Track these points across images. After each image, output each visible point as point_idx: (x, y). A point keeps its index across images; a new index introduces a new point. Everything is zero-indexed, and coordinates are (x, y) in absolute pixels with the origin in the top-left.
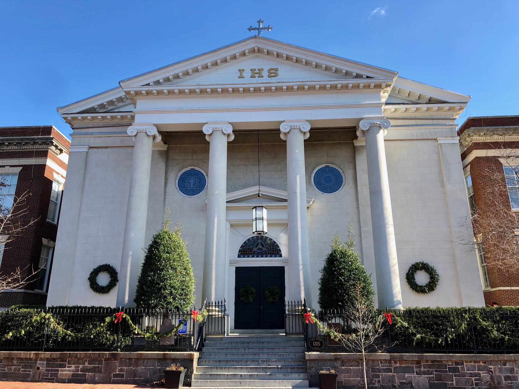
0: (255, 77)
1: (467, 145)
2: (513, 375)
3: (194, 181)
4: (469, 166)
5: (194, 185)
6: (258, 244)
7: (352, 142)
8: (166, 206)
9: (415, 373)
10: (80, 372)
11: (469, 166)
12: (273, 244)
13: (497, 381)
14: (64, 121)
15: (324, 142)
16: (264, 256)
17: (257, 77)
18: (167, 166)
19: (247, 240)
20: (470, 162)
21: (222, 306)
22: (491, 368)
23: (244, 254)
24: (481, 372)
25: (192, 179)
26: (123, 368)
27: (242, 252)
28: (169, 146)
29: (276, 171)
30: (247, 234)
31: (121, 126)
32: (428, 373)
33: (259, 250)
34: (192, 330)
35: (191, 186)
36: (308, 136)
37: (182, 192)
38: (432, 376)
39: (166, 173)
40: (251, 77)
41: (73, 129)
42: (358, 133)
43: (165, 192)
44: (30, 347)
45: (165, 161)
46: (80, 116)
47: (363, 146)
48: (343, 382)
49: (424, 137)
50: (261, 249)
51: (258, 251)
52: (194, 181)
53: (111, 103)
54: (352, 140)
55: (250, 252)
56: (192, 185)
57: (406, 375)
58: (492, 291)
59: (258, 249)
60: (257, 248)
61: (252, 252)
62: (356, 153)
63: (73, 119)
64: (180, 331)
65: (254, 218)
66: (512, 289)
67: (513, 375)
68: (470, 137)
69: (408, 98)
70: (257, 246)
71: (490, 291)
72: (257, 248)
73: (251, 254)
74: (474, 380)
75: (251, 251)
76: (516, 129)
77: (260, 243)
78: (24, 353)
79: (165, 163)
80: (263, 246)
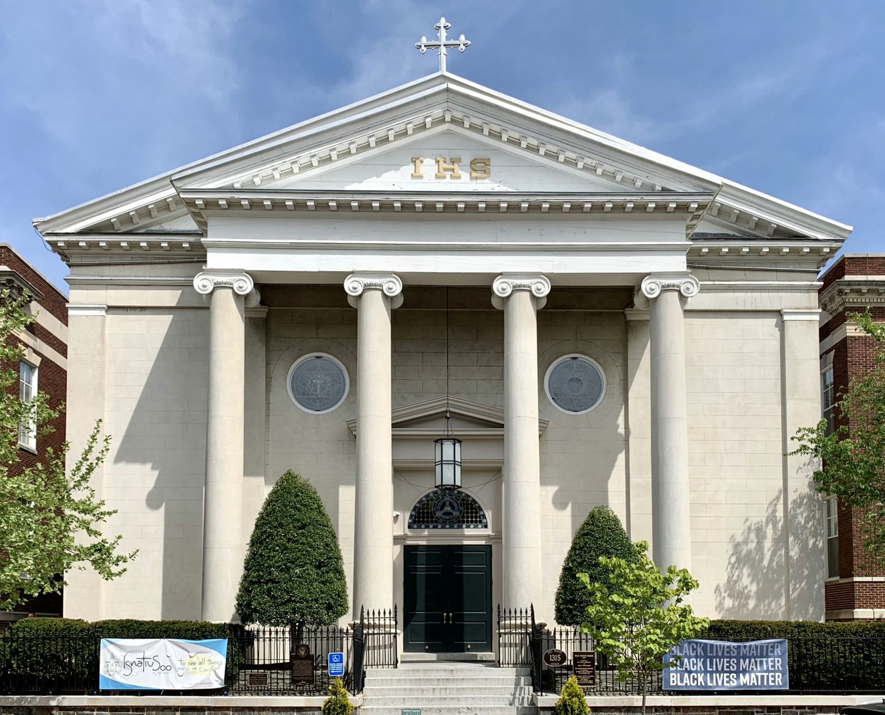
0: (444, 177)
1: (834, 311)
3: (322, 382)
4: (833, 352)
5: (322, 389)
6: (444, 505)
7: (624, 312)
8: (270, 430)
11: (833, 352)
12: (471, 504)
14: (50, 248)
15: (570, 310)
16: (456, 526)
17: (448, 177)
18: (267, 350)
19: (425, 497)
20: (837, 344)
23: (419, 522)
25: (319, 377)
27: (415, 518)
28: (269, 310)
29: (479, 365)
30: (424, 488)
31: (169, 263)
33: (446, 515)
35: (316, 392)
36: (544, 303)
37: (299, 403)
39: (268, 364)
40: (437, 177)
41: (70, 266)
42: (637, 301)
43: (268, 403)
45: (264, 340)
46: (83, 241)
47: (645, 320)
48: (426, 554)
49: (756, 307)
50: (450, 514)
51: (444, 517)
52: (322, 382)
53: (146, 212)
54: (624, 309)
55: (430, 520)
56: (318, 390)
58: (840, 584)
59: (445, 514)
60: (443, 512)
61: (434, 519)
62: (629, 335)
63: (69, 244)
64: (333, 672)
65: (438, 459)
66: (874, 580)
68: (840, 296)
69: (735, 223)
70: (442, 508)
71: (837, 583)
72: (443, 512)
73: (432, 522)
75: (432, 517)
77: (448, 503)
78: (31, 698)
79: (265, 345)
80: (453, 508)
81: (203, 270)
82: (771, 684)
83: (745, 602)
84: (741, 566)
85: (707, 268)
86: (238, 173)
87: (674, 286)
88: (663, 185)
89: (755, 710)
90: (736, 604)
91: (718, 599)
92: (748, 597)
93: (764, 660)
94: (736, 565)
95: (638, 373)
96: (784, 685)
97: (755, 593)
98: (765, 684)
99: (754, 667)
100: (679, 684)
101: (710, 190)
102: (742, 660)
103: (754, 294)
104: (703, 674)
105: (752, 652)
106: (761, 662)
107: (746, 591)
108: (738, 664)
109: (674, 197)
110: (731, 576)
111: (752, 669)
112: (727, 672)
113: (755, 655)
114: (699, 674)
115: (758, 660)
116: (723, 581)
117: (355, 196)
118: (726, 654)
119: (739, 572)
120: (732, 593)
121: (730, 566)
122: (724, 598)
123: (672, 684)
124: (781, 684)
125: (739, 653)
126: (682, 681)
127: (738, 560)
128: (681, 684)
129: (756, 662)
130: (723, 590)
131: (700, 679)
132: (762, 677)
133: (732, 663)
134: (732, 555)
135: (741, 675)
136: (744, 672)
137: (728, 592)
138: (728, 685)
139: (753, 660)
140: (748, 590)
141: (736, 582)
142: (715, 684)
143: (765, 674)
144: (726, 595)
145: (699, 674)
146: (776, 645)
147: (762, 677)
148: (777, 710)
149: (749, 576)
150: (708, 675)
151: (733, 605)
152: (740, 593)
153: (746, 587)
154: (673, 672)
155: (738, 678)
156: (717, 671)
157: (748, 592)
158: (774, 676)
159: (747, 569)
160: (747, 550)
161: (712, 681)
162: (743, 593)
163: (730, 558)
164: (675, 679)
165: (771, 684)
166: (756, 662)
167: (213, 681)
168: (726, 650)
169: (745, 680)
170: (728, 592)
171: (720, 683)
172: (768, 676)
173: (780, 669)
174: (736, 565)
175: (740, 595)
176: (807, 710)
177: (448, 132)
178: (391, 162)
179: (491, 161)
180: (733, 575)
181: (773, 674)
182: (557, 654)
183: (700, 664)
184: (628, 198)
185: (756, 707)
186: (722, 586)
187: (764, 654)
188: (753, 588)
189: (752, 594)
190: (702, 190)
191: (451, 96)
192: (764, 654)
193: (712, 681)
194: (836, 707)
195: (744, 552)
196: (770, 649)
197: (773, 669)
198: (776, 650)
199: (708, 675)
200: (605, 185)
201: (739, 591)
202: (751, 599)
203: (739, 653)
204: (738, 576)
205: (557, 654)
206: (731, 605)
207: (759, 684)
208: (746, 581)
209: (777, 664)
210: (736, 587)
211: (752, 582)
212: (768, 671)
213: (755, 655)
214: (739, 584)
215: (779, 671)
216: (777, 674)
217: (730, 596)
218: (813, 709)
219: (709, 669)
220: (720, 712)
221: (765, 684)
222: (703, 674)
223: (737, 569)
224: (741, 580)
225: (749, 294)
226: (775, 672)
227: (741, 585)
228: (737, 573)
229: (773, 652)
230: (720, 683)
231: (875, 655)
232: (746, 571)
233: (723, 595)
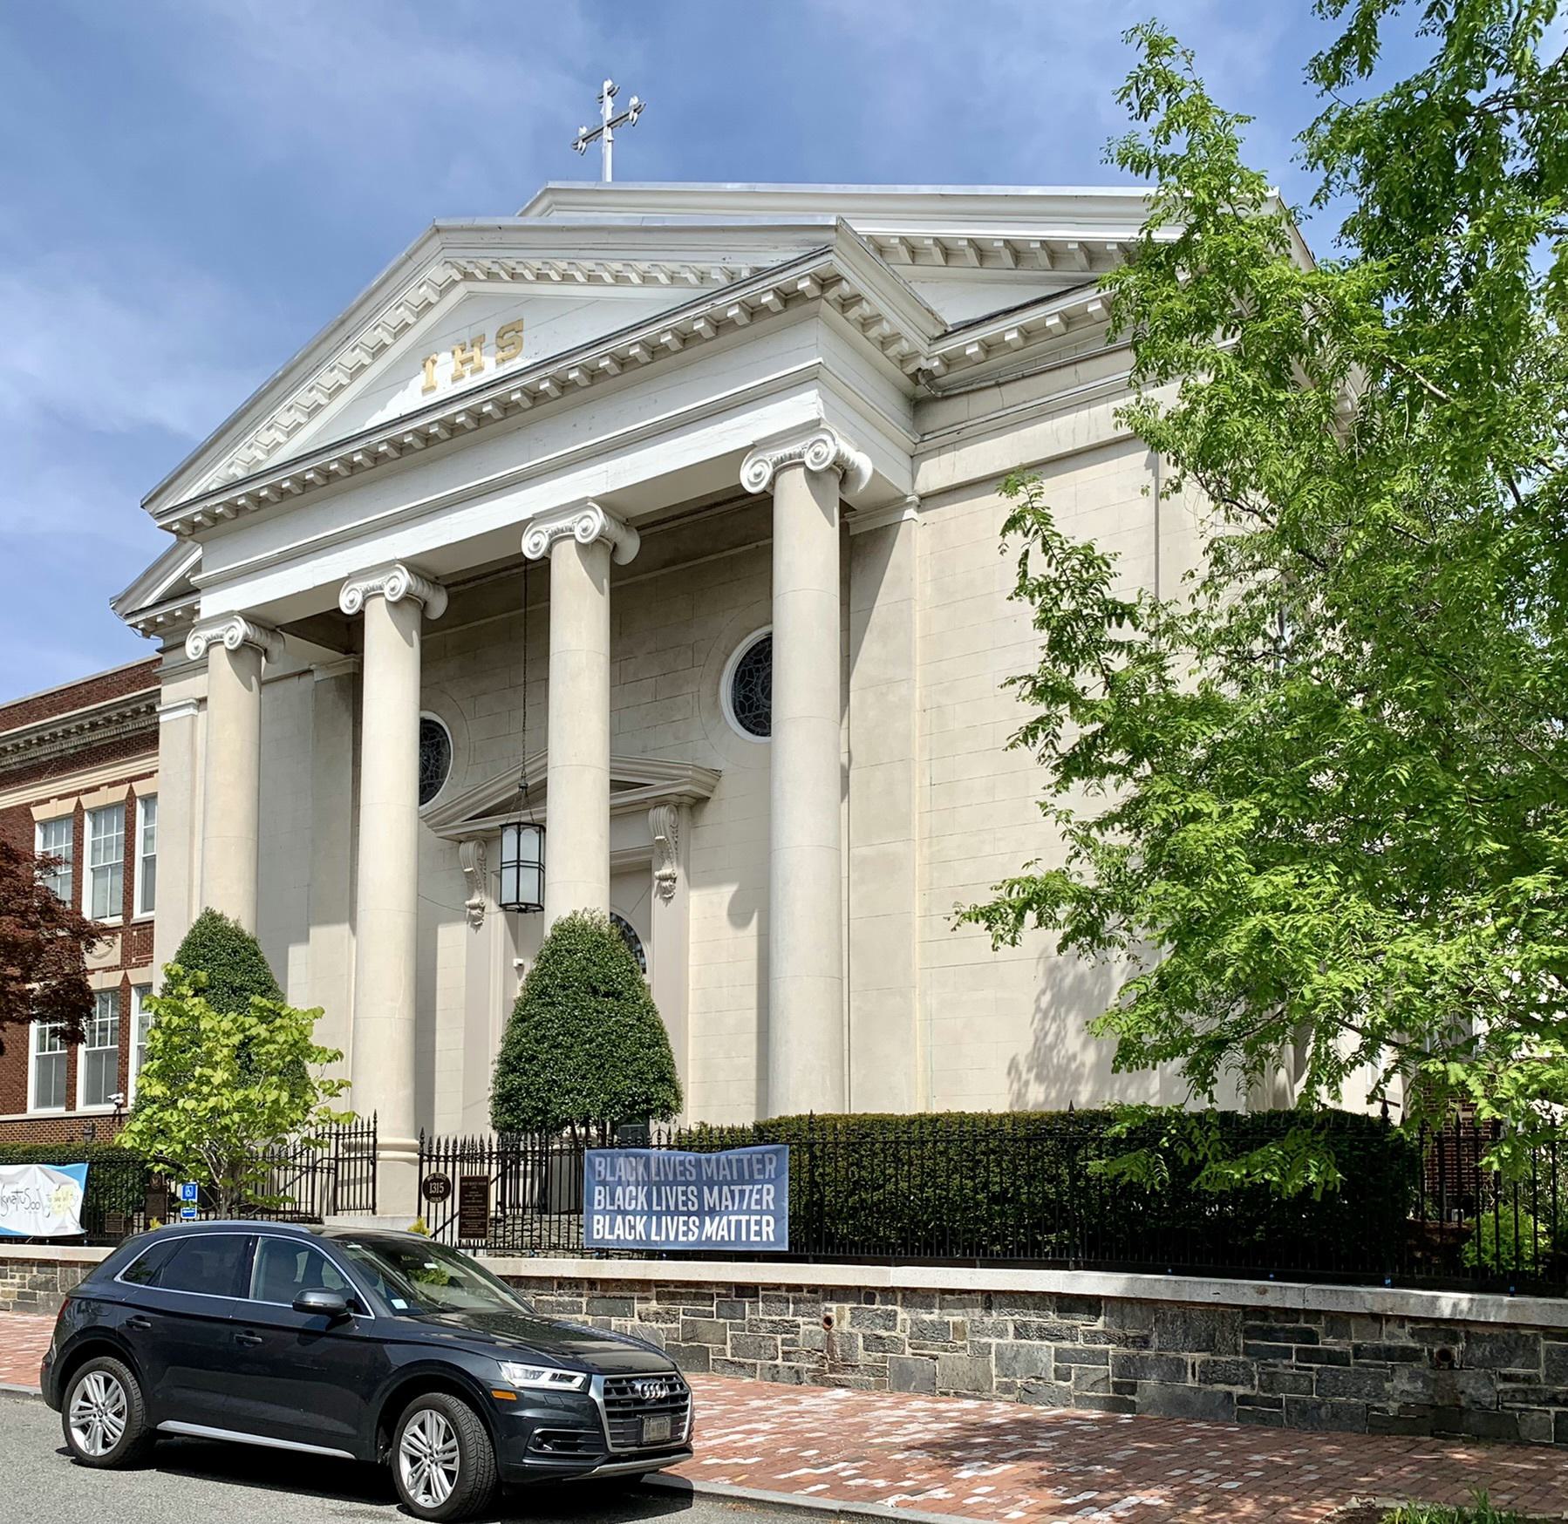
2: (893, 1334)
9: (636, 1317)
10: (990, 1345)
13: (842, 1350)
21: (368, 1133)
22: (830, 1310)
24: (800, 1320)
26: (1542, 1355)
32: (667, 1316)
34: (339, 1189)
38: (674, 1325)
44: (1053, 1255)
57: (614, 1321)
67: (893, 1334)
74: (779, 1343)
76: (523, 802)
81: (194, 626)
82: (753, 1238)
83: (1072, 1089)
84: (1063, 1010)
85: (998, 385)
86: (211, 468)
87: (791, 457)
88: (751, 265)
89: (714, 1291)
90: (1053, 1094)
91: (1015, 1086)
92: (1077, 1078)
93: (747, 1188)
94: (1052, 1013)
95: (867, 637)
96: (778, 1241)
97: (1091, 1069)
98: (744, 1238)
99: (729, 1203)
100: (608, 1237)
101: (822, 243)
102: (706, 1189)
103: (1092, 410)
104: (645, 1218)
105: (722, 1172)
106: (742, 1192)
107: (1073, 1066)
108: (700, 1197)
109: (766, 282)
110: (1042, 1035)
111: (727, 1207)
112: (683, 1213)
113: (729, 1178)
114: (638, 1218)
115: (736, 1188)
116: (1023, 1046)
117: (332, 453)
118: (679, 1178)
119: (1059, 1026)
120: (1045, 1072)
121: (1038, 1016)
122: (1027, 1083)
123: (596, 1237)
124: (772, 1239)
125: (699, 1174)
126: (612, 1232)
127: (1057, 1001)
128: (610, 1237)
129: (732, 1192)
130: (1023, 1068)
131: (640, 1228)
132: (739, 1223)
133: (690, 1196)
134: (1043, 992)
135: (707, 1219)
136: (712, 1212)
137: (1035, 1071)
138: (685, 1239)
139: (725, 1188)
140: (1078, 1061)
141: (1051, 1048)
142: (663, 1238)
143: (744, 1218)
144: (1032, 1076)
145: (638, 1218)
146: (767, 1157)
147: (739, 1223)
148: (750, 1292)
149: (1079, 1031)
150: (654, 1218)
151: (1047, 1097)
152: (1062, 1070)
153: (1074, 1057)
154: (598, 1213)
155: (701, 1226)
156: (668, 1212)
157: (1077, 1068)
158: (758, 1223)
159: (1076, 1017)
160: (1075, 977)
161: (659, 1233)
162: (1066, 1069)
163: (1038, 999)
164: (600, 1227)
165: (753, 1238)
166: (732, 1192)
167: (68, 1224)
168: (679, 1169)
169: (716, 1231)
170: (1035, 1071)
171: (672, 1238)
172: (748, 1222)
173: (772, 1207)
174: (1052, 1013)
175: (1062, 1075)
176: (805, 1294)
177: (471, 297)
178: (395, 380)
179: (525, 322)
180: (1046, 1034)
181: (758, 1218)
182: (440, 1181)
183: (642, 1198)
184: (691, 313)
185: (717, 1284)
186: (1021, 1059)
187: (747, 1177)
188: (1090, 1057)
189: (1087, 1070)
190: (811, 249)
191: (443, 236)
192: (747, 1177)
193: (659, 1233)
194: (859, 1288)
195: (1068, 981)
196: (756, 1167)
197: (758, 1207)
198: (768, 1167)
199: (654, 1218)
200: (663, 297)
201: (1059, 1066)
202: (1084, 1082)
203: (699, 1174)
204: (1057, 1035)
205: (440, 1181)
206: (1041, 1098)
207: (733, 1238)
208: (1073, 1043)
209: (765, 1197)
210: (1051, 1058)
211: (1085, 1046)
212: (749, 1212)
213: (729, 1178)
214: (1059, 1052)
215: (768, 1212)
216: (765, 1218)
217: (1040, 1078)
218: (816, 1292)
219: (655, 1208)
220: (658, 1293)
221: (744, 1238)
222: (645, 1218)
223: (1054, 1019)
224: (1063, 1041)
225: (1084, 414)
226: (761, 1213)
227: (1063, 1052)
228: (1054, 1028)
229: (762, 1171)
230: (672, 1238)
231: (998, 1179)
232: (1073, 1022)
233: (1024, 1076)
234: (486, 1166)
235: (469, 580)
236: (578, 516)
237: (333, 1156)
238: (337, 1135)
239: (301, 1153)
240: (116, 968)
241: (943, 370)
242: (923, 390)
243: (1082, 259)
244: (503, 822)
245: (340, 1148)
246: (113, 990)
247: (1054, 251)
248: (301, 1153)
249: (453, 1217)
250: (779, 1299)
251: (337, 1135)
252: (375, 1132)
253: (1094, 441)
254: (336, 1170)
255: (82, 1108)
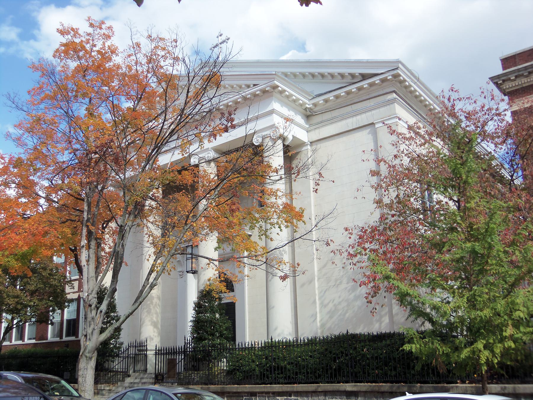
89: (244, 395)
176: (271, 395)
225: (355, 118)
234: (178, 356)
235: (417, 112)
236: (207, 153)
237: (134, 353)
238: (135, 346)
239: (128, 348)
240: (76, 292)
241: (313, 107)
242: (309, 113)
243: (350, 77)
244: (187, 245)
245: (136, 350)
246: (76, 299)
247: (342, 76)
248: (126, 350)
249: (182, 359)
250: (263, 396)
251: (135, 346)
252: (146, 346)
253: (358, 126)
254: (135, 358)
255: (65, 339)
